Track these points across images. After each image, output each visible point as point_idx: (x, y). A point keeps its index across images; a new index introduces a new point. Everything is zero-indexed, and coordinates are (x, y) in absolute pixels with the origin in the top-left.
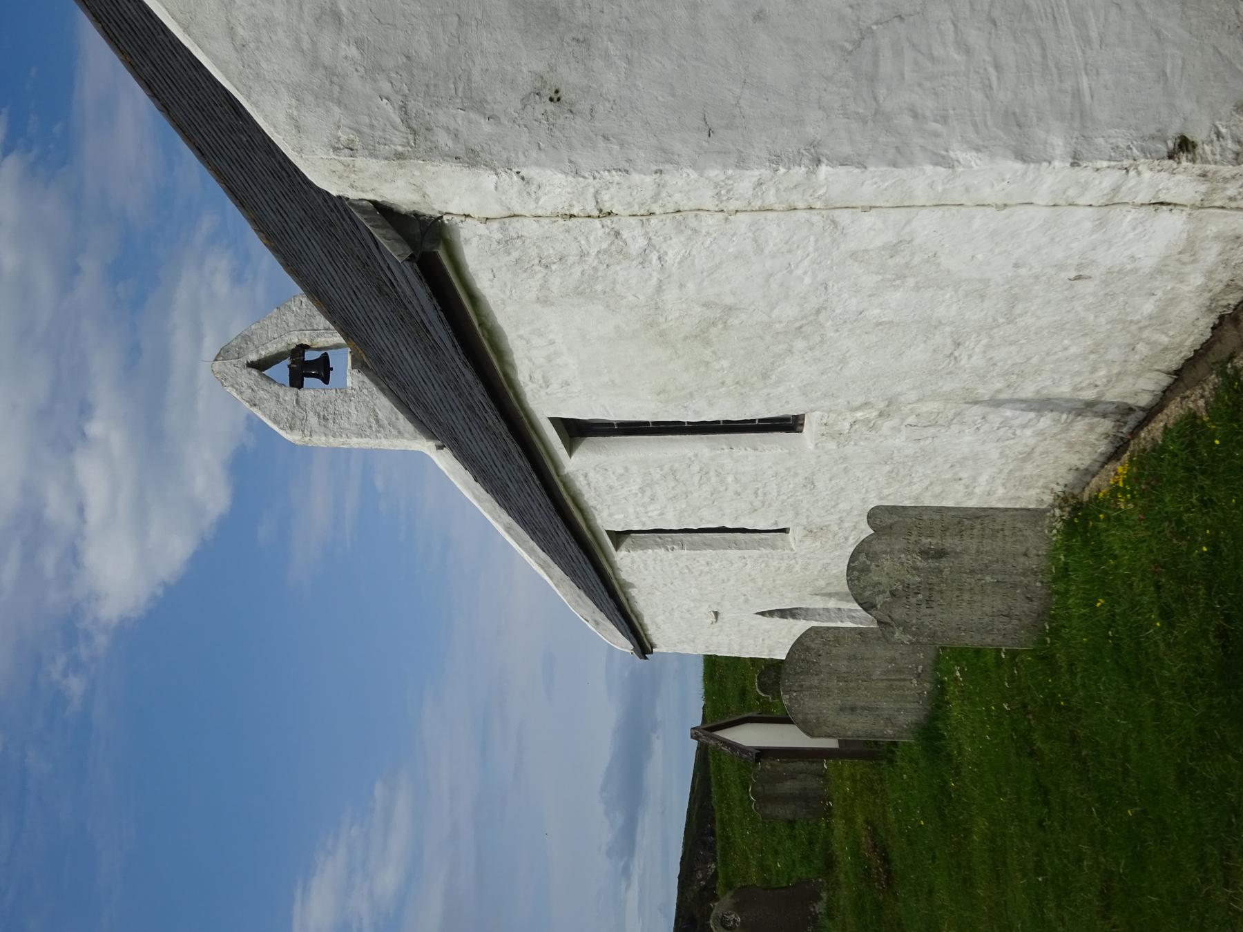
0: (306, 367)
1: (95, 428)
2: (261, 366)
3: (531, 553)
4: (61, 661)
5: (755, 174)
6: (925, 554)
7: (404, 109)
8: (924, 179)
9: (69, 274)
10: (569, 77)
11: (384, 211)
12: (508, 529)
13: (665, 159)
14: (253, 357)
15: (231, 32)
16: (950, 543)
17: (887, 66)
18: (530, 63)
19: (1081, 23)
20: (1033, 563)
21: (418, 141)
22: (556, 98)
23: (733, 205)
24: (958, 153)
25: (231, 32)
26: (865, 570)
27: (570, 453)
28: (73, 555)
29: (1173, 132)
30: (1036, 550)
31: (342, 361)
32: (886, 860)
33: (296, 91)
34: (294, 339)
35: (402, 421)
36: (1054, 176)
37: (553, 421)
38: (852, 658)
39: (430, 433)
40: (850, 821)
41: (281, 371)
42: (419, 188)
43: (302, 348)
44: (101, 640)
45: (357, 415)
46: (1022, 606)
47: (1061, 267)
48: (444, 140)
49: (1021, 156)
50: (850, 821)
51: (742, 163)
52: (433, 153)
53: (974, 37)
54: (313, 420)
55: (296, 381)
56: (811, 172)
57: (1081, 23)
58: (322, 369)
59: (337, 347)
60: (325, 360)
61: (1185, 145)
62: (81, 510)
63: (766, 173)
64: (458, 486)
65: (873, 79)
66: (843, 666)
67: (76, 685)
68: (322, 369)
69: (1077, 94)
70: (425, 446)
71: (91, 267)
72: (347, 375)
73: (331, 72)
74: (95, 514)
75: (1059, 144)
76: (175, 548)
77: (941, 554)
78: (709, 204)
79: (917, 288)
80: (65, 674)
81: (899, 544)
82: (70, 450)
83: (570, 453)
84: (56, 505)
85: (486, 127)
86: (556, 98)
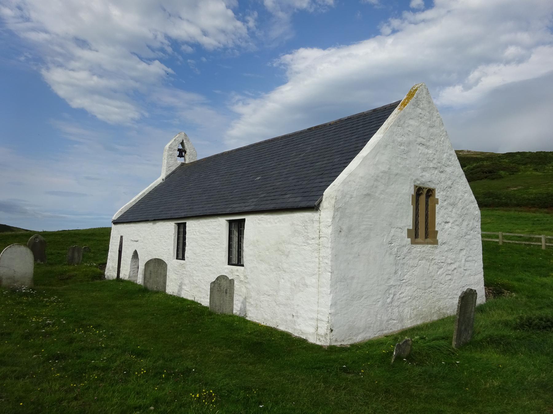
0: (182, 153)
1: (95, 78)
2: (182, 143)
3: (138, 198)
4: (30, 56)
5: (330, 263)
6: (226, 290)
7: (340, 208)
8: (327, 290)
9: (136, 80)
10: (343, 234)
11: (321, 201)
12: (144, 193)
13: (332, 249)
14: (184, 141)
15: (350, 181)
16: (228, 294)
17: (342, 283)
18: (345, 227)
19: (346, 314)
20: (224, 311)
21: (340, 210)
22: (340, 232)
23: (321, 259)
24: (331, 295)
25: (350, 181)
26: (224, 279)
27: (227, 220)
28: (60, 66)
29: (334, 329)
30: (227, 311)
31: (180, 161)
32: (67, 279)
33: (343, 191)
34: (188, 151)
35: (170, 172)
36: (327, 310)
37: (244, 220)
38: (161, 274)
39: (168, 177)
40: (74, 270)
41: (181, 147)
42: (327, 208)
43: (185, 152)
44: (35, 68)
45: (172, 162)
46: (217, 308)
47: (297, 312)
48: (336, 213)
49: (331, 305)
50: (74, 270)
51: (331, 261)
52: (335, 212)
53: (345, 297)
54: (171, 153)
55: (179, 150)
56: (329, 272)
57: (346, 314)
58: (181, 155)
59: (185, 160)
60: (183, 156)
61: (332, 331)
62: (73, 70)
63: (330, 265)
64: (154, 183)
65: (341, 281)
66: (159, 271)
67: (22, 59)
68: (181, 155)
69: (338, 313)
70: (163, 176)
71: (137, 85)
72: (180, 161)
73: (345, 196)
74: (72, 73)
75: (333, 311)
76: (62, 92)
77: (226, 293)
78: (321, 255)
79: (291, 288)
80: (26, 56)
81: (228, 285)
82: (90, 71)
83: (227, 220)
84: (74, 64)
85: (337, 220)
86: (340, 232)
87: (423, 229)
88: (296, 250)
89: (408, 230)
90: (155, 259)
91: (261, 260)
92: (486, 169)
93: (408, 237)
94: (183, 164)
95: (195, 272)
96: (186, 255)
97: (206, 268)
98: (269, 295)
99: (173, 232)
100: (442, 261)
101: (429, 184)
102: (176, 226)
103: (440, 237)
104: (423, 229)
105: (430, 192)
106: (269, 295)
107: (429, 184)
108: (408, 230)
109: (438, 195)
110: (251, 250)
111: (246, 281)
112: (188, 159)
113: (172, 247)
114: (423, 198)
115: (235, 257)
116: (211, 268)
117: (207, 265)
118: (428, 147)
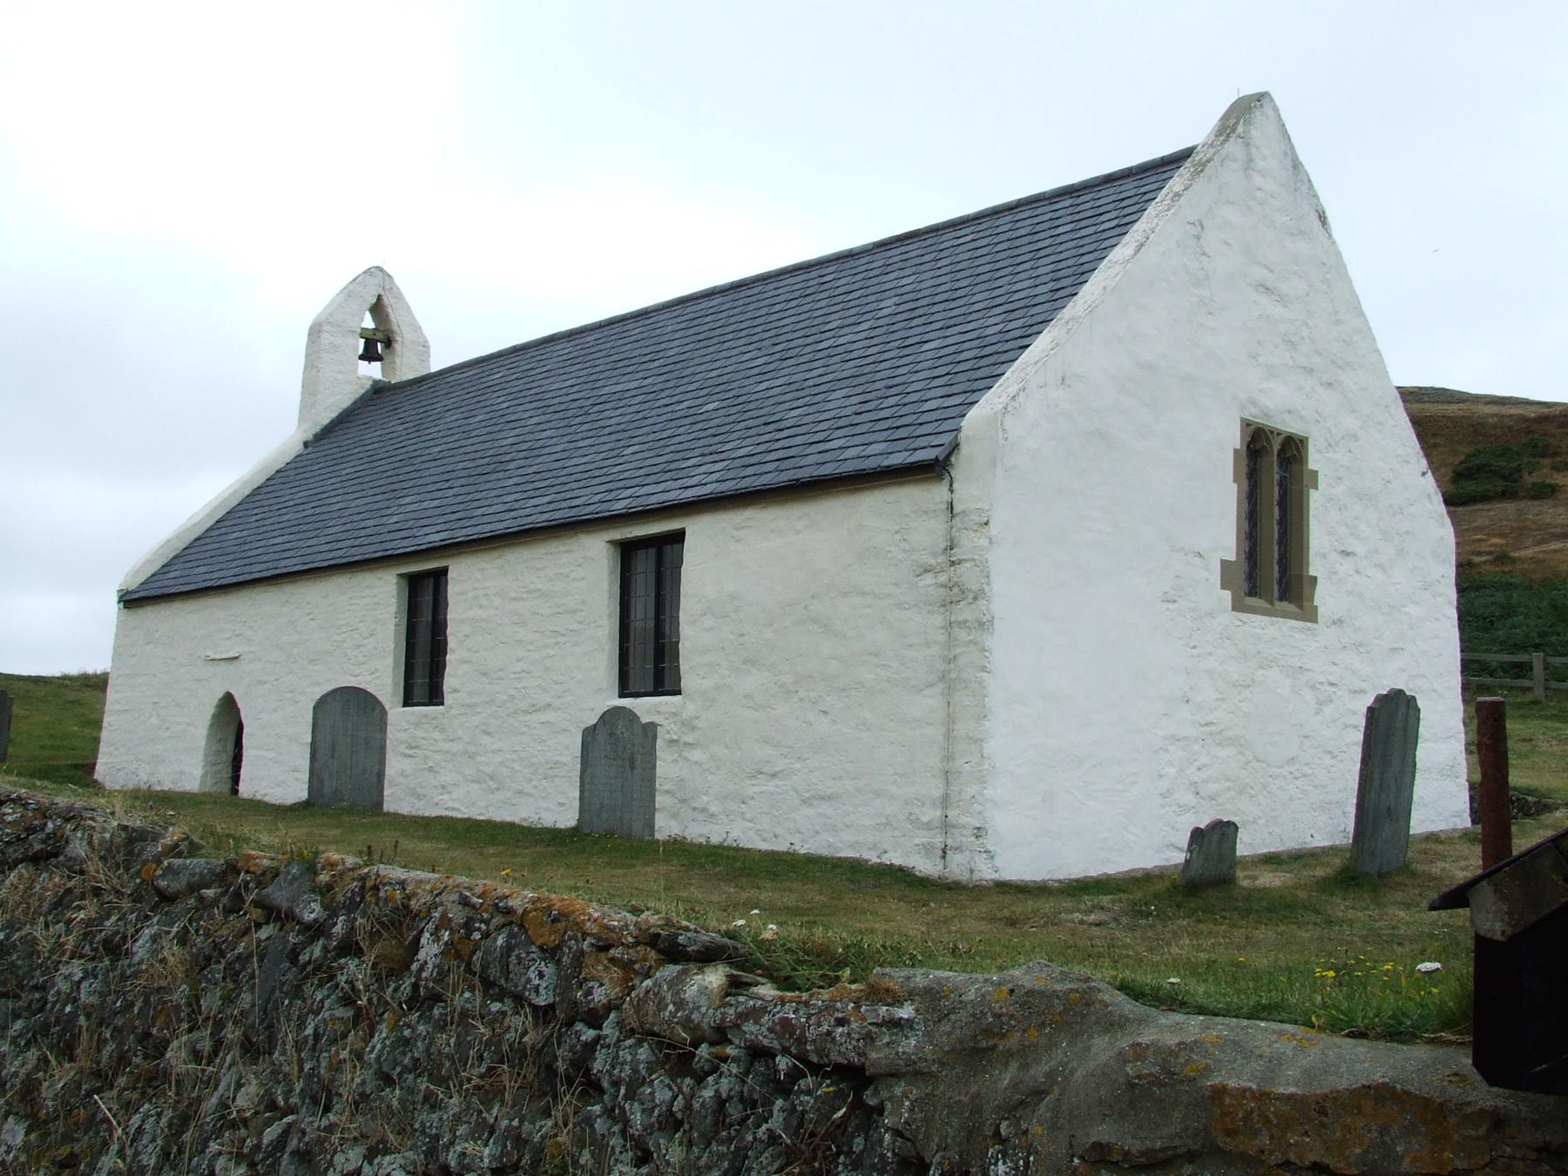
31: (373, 371)
37: (678, 537)
58: (369, 355)
60: (379, 358)
83: (612, 542)
87: (1272, 567)
88: (869, 611)
89: (1224, 563)
90: (315, 708)
91: (746, 662)
92: (1559, 530)
93: (1223, 587)
94: (378, 391)
95: (485, 739)
96: (450, 681)
97: (534, 717)
98: (774, 775)
99: (393, 609)
100: (1332, 679)
101: (1287, 417)
102: (404, 583)
103: (1325, 598)
104: (1272, 567)
105: (1292, 450)
106: (774, 775)
107: (1287, 417)
108: (1224, 563)
109: (1315, 461)
110: (707, 630)
111: (689, 739)
112: (406, 369)
113: (390, 661)
114: (1273, 472)
115: (649, 657)
116: (549, 716)
117: (535, 709)
118: (1281, 299)
